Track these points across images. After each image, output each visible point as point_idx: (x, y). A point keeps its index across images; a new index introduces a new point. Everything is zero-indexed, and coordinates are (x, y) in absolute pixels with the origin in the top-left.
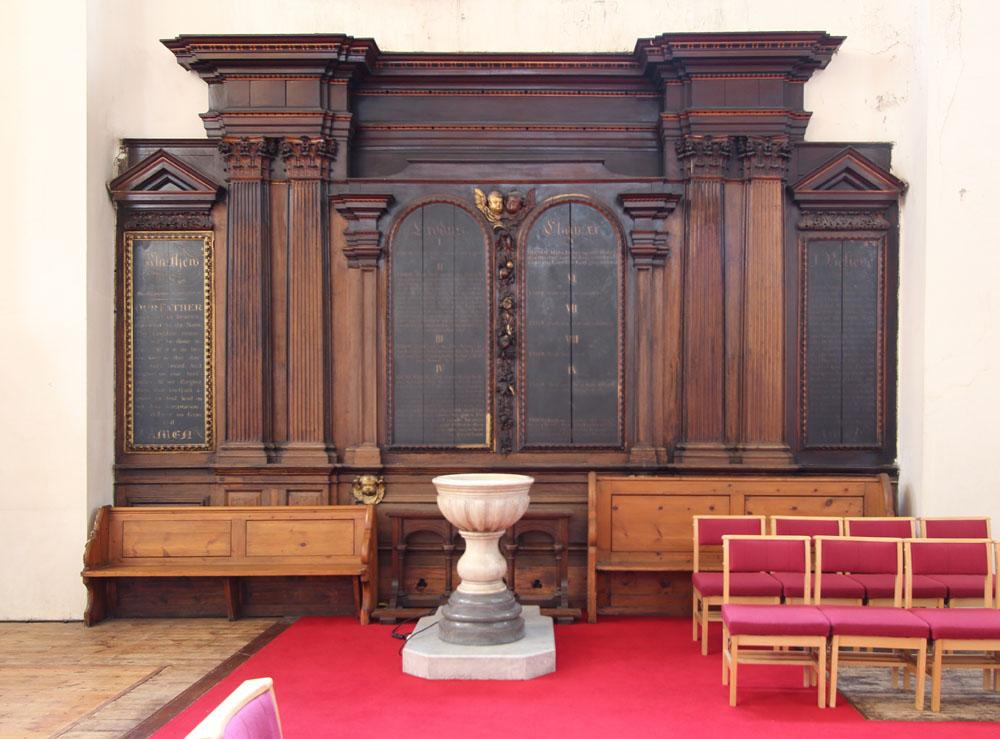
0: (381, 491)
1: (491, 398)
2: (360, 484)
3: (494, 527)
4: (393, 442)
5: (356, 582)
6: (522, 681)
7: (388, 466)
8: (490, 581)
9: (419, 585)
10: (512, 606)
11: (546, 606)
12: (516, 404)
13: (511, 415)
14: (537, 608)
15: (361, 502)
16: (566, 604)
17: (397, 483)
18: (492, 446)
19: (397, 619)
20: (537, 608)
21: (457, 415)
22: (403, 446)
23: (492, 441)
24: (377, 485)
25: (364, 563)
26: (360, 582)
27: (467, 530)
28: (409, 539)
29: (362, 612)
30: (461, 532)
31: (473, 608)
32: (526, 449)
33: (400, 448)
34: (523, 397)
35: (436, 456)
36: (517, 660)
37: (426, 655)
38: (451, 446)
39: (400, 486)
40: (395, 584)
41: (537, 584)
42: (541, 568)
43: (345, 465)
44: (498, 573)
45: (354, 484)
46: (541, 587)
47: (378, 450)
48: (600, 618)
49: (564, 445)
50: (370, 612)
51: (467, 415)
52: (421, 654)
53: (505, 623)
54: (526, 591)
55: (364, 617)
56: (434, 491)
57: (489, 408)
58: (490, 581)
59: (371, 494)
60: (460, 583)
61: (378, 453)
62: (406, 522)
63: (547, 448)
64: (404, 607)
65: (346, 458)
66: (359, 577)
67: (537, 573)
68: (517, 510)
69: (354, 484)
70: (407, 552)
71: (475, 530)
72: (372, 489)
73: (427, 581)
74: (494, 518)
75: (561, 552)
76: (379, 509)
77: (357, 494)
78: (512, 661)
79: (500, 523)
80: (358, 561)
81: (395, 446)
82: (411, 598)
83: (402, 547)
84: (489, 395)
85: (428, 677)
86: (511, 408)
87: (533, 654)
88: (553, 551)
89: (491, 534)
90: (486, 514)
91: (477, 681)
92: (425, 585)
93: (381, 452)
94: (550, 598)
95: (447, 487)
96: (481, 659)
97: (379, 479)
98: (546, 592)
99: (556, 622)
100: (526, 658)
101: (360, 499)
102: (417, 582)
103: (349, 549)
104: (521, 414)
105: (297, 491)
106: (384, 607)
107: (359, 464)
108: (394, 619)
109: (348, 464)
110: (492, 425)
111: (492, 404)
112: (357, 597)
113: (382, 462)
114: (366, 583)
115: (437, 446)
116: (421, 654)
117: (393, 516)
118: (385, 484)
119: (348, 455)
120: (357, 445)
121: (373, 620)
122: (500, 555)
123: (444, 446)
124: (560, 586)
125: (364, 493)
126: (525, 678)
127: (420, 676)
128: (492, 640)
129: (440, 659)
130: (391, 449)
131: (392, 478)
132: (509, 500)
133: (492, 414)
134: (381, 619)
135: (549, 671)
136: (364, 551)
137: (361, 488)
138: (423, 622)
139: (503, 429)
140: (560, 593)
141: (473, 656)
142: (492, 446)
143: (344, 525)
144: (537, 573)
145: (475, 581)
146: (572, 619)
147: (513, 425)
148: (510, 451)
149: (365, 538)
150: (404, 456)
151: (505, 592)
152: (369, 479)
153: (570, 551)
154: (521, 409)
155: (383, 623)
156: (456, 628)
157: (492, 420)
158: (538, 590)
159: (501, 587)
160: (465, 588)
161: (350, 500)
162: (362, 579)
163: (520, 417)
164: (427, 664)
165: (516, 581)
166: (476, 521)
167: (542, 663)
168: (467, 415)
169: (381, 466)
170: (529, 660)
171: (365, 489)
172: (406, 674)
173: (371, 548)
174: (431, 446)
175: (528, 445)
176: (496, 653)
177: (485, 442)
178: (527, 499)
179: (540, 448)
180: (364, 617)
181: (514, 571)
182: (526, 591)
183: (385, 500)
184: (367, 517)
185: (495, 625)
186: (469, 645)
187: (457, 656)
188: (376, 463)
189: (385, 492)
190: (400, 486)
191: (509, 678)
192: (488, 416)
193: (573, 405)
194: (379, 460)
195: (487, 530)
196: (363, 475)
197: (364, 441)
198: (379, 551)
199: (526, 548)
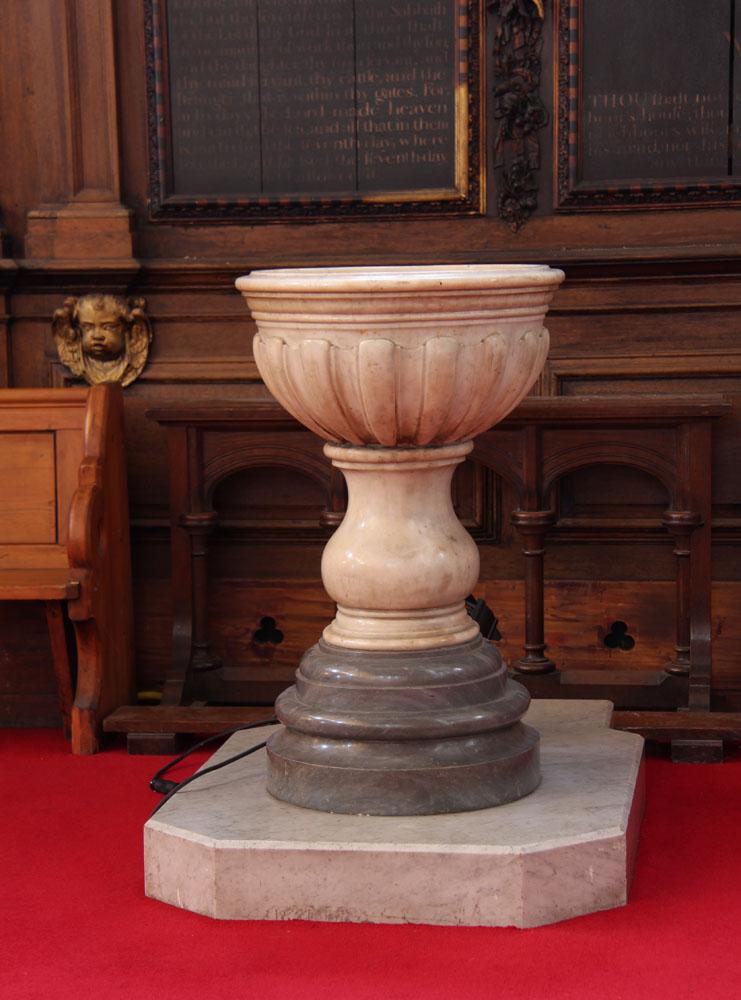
0: (140, 345)
1: (471, 32)
2: (74, 322)
3: (427, 432)
4: (171, 188)
5: (56, 623)
6: (512, 929)
7: (157, 265)
8: (420, 608)
9: (259, 636)
10: (494, 689)
11: (629, 705)
12: (551, 48)
13: (536, 87)
14: (602, 707)
15: (81, 381)
16: (706, 700)
17: (182, 320)
18: (473, 192)
19: (179, 736)
20: (602, 707)
21: (362, 94)
22: (201, 199)
23: (472, 178)
24: (124, 325)
25: (76, 562)
26: (68, 624)
27: (344, 443)
28: (225, 492)
29: (75, 715)
30: (330, 451)
31: (364, 695)
32: (580, 203)
33: (192, 207)
34: (572, 24)
35: (302, 231)
36: (494, 862)
37: (209, 843)
38: (345, 196)
39: (197, 328)
40: (182, 630)
41: (616, 636)
42: (631, 587)
43: (27, 263)
44: (447, 579)
45: (56, 323)
46: (629, 644)
47: (124, 212)
48: (193, 556)
49: (703, 182)
50: (97, 715)
51: (394, 93)
52: (195, 837)
53: (471, 743)
54: (585, 657)
55: (80, 730)
56: (242, 324)
57: (462, 67)
58: (420, 608)
59: (109, 354)
60: (330, 619)
61: (124, 225)
62: (211, 439)
63: (647, 195)
64: (210, 704)
65: (30, 241)
66: (63, 604)
67: (618, 601)
68: (499, 372)
69: (56, 323)
70: (218, 537)
71: (368, 442)
72: (109, 336)
73: (281, 625)
74: (423, 399)
75: (688, 530)
76: (128, 400)
77: (65, 351)
78: (479, 867)
79: (446, 417)
80: (60, 559)
81: (174, 199)
82: (231, 673)
83: (198, 517)
84: (462, 21)
85: (215, 912)
86: (536, 65)
87: (546, 846)
88: (663, 530)
89: (420, 453)
90: (396, 385)
91: (368, 926)
92: (278, 636)
93: (135, 223)
94: (657, 679)
95: (273, 295)
96: (378, 855)
97: (131, 306)
98: (645, 662)
99: (657, 752)
100: (525, 858)
101: (78, 368)
102: (254, 627)
103: (40, 523)
104: (565, 84)
105: (617, 543)
106: (155, 702)
107: (69, 257)
108: (171, 736)
109: (37, 260)
110: (473, 125)
111: (472, 52)
112: (62, 669)
113: (137, 252)
114: (85, 626)
115: (304, 197)
116: (195, 837)
117: (171, 419)
118: (150, 323)
119: (35, 231)
120: (60, 200)
121: (109, 740)
122: (455, 526)
123: (326, 197)
124: (687, 641)
125: (88, 353)
126: (520, 924)
127: (192, 907)
128: (423, 795)
129: (254, 852)
130: (167, 211)
131: (172, 304)
132: (472, 338)
133: (472, 89)
134: (131, 736)
135: (606, 904)
136: (76, 527)
137: (78, 337)
138: (239, 741)
139: (507, 136)
140: (686, 664)
141: (355, 847)
142: (473, 192)
143: (27, 447)
144: (618, 601)
145: (375, 607)
146: (718, 743)
147: (539, 120)
148: (532, 209)
149: (81, 489)
150: (207, 233)
151: (471, 644)
152: (101, 308)
153: (715, 530)
154: (564, 65)
155: (138, 748)
156: (313, 758)
157: (472, 106)
158: (622, 655)
159: (459, 629)
160: (351, 631)
161: (49, 374)
162: (73, 613)
163: (563, 92)
164: (208, 870)
165: (550, 627)
166: (366, 405)
167: (580, 876)
168: (394, 93)
169: (131, 264)
170: (535, 865)
171: (89, 336)
172: (155, 903)
173: (97, 520)
174: (285, 198)
175: (586, 186)
176: (430, 839)
177: (448, 181)
178: (535, 339)
179: (626, 196)
180: (80, 730)
181: (541, 597)
182: (585, 657)
183: (149, 374)
184: (86, 425)
185: (438, 749)
186: (353, 812)
187: (303, 846)
188: (119, 255)
189: (151, 347)
190: (197, 328)
191: (470, 920)
192: (461, 95)
193: (729, 37)
194: (126, 247)
195: (405, 440)
196: (80, 294)
197: (79, 186)
198: (135, 531)
199: (583, 522)
